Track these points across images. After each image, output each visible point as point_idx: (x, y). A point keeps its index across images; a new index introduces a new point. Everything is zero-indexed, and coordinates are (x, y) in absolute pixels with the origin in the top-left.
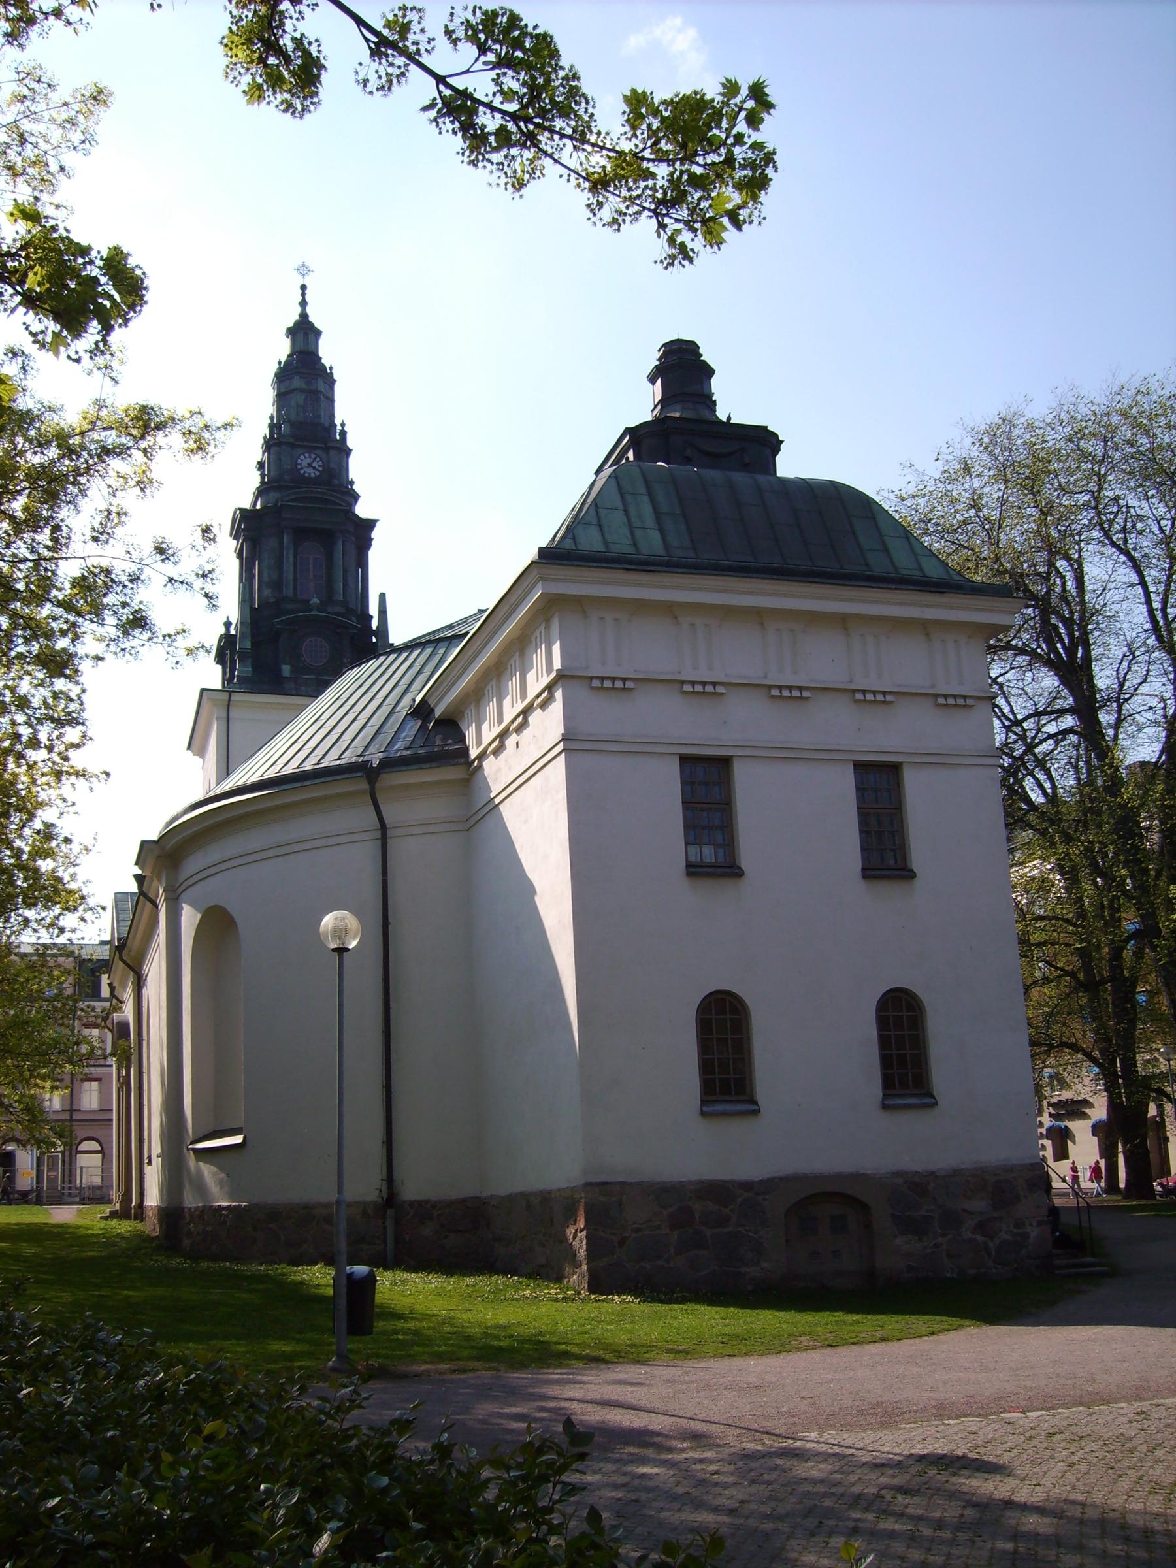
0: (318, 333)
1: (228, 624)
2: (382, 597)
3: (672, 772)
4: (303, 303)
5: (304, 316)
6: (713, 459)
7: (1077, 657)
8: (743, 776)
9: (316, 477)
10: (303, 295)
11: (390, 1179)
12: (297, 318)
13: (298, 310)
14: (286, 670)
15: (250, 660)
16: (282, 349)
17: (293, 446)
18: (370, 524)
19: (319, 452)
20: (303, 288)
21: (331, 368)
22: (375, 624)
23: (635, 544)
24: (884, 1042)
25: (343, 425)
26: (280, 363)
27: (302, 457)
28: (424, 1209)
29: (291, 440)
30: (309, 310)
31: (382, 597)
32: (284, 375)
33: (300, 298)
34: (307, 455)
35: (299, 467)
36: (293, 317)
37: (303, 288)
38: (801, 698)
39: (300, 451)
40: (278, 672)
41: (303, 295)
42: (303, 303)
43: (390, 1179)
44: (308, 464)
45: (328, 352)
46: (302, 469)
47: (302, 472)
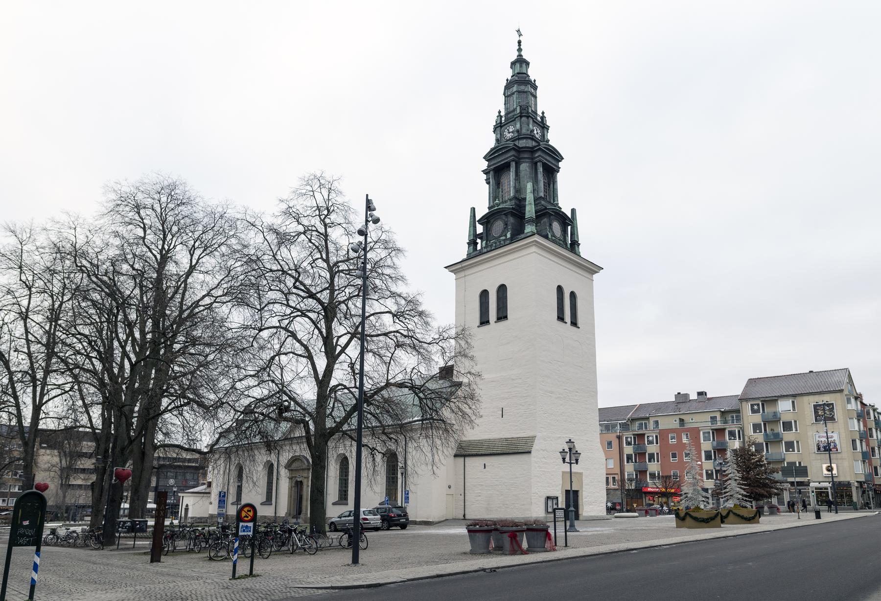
0: (528, 64)
1: (500, 112)
4: (520, 50)
5: (520, 55)
12: (516, 58)
13: (517, 53)
16: (508, 74)
20: (519, 42)
21: (535, 81)
25: (543, 113)
26: (507, 80)
30: (522, 53)
32: (509, 85)
36: (514, 57)
37: (519, 42)
42: (520, 50)
45: (533, 73)
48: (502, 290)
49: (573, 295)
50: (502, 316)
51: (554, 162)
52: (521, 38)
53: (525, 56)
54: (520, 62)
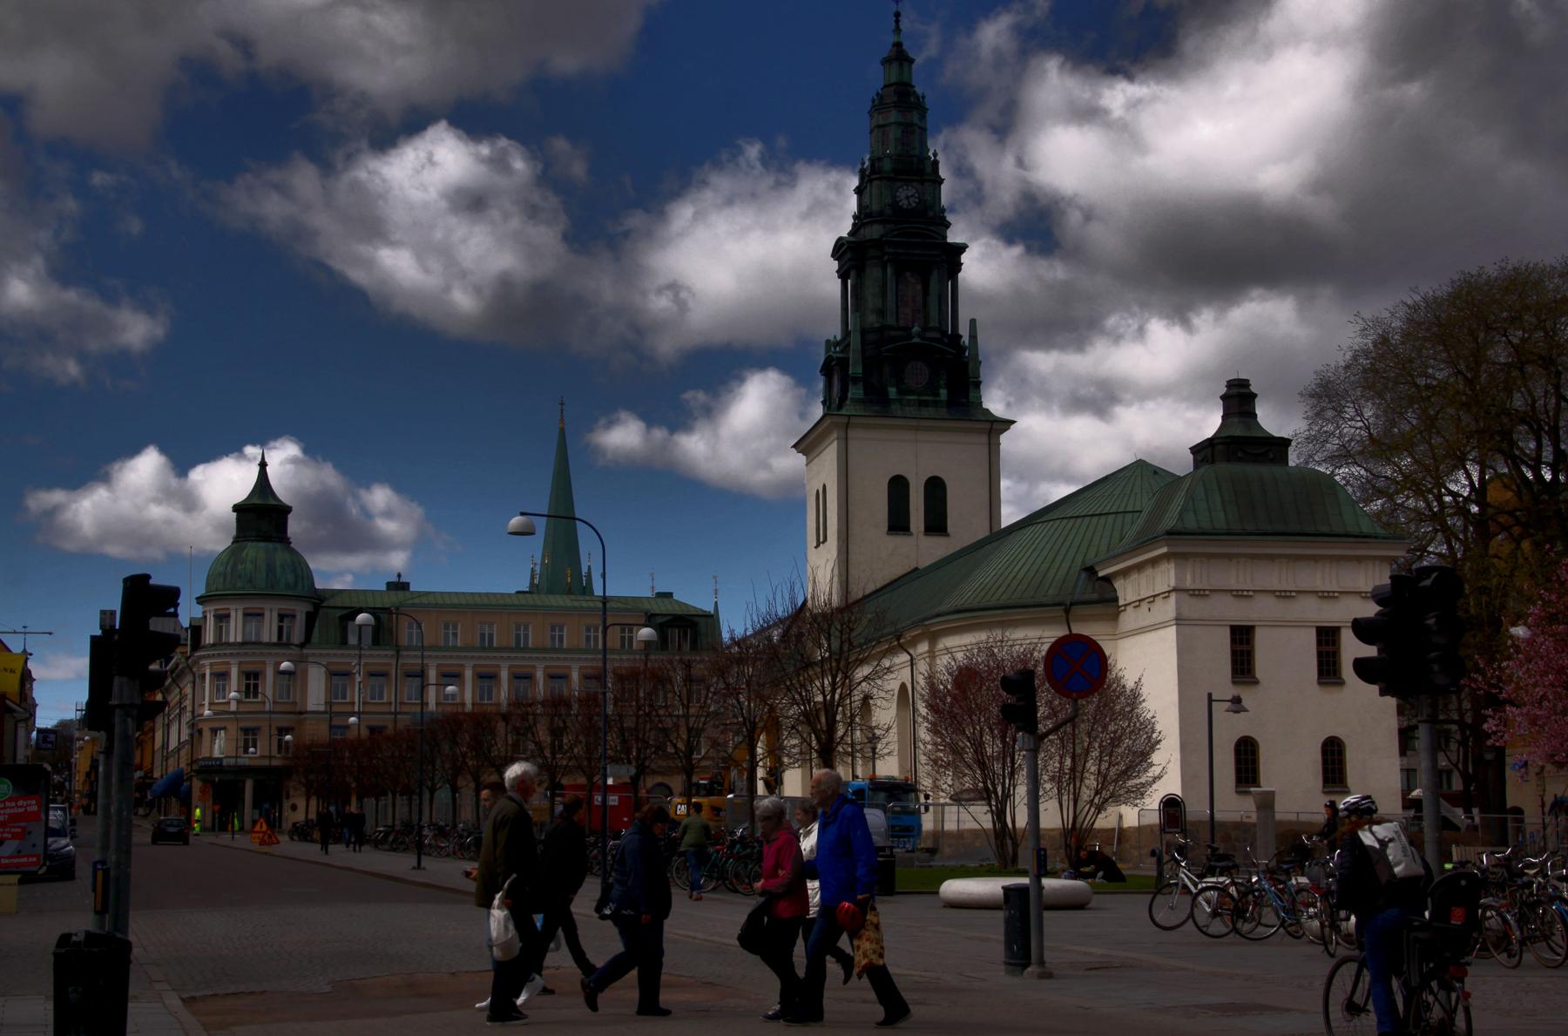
2: (973, 322)
3: (1227, 632)
5: (898, 45)
6: (1257, 459)
7: (864, 898)
8: (1260, 637)
11: (1228, 701)
14: (892, 392)
15: (861, 383)
19: (915, 184)
21: (923, 97)
23: (1212, 521)
24: (1325, 762)
27: (901, 190)
29: (892, 175)
31: (973, 322)
34: (905, 187)
35: (898, 199)
36: (886, 51)
38: (1291, 596)
39: (899, 184)
40: (886, 393)
41: (897, 22)
43: (1228, 701)
44: (907, 195)
46: (901, 201)
47: (901, 204)
48: (824, 486)
49: (936, 488)
50: (825, 540)
51: (483, 662)
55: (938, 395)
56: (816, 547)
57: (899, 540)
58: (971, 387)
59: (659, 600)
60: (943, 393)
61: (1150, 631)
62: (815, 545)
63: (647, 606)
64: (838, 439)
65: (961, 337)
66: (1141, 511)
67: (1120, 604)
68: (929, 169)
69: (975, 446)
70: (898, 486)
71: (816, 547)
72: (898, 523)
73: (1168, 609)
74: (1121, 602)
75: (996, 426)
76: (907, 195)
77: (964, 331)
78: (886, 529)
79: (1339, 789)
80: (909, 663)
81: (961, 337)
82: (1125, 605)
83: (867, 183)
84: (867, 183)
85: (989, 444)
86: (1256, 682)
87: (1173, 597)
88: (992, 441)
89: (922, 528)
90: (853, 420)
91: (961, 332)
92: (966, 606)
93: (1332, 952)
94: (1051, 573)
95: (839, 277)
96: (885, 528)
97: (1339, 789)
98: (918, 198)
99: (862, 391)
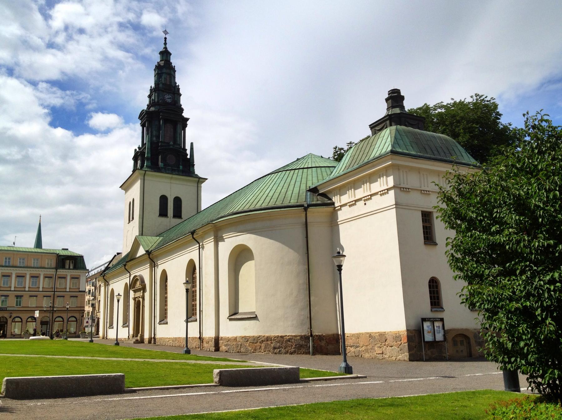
2: (192, 144)
4: (165, 44)
5: (166, 48)
9: (170, 103)
10: (165, 41)
13: (163, 46)
17: (163, 91)
18: (187, 119)
19: (171, 94)
20: (165, 38)
22: (188, 157)
27: (166, 95)
28: (320, 338)
30: (167, 46)
31: (192, 144)
33: (164, 42)
36: (162, 49)
37: (165, 38)
41: (165, 41)
42: (165, 44)
44: (168, 98)
45: (174, 61)
48: (133, 200)
49: (178, 201)
50: (133, 218)
52: (167, 36)
53: (169, 49)
54: (165, 54)
55: (179, 168)
56: (128, 223)
57: (163, 219)
58: (191, 166)
59: (63, 251)
60: (181, 167)
61: (52, 327)
62: (128, 222)
63: (58, 252)
64: (141, 179)
65: (186, 150)
66: (335, 167)
67: (336, 206)
68: (176, 90)
69: (192, 187)
70: (163, 200)
71: (128, 223)
72: (163, 213)
73: (390, 198)
74: (336, 205)
75: (201, 180)
76: (168, 98)
77: (188, 147)
78: (158, 215)
79: (6, 328)
80: (198, 248)
81: (186, 150)
82: (341, 206)
83: (153, 92)
84: (153, 92)
85: (198, 186)
86: (436, 244)
87: (392, 193)
88: (199, 186)
89: (172, 215)
90: (147, 172)
91: (186, 148)
92: (240, 210)
93: (28, 320)
94: (289, 193)
95: (141, 126)
96: (158, 213)
97: (6, 328)
98: (172, 99)
99: (150, 163)
